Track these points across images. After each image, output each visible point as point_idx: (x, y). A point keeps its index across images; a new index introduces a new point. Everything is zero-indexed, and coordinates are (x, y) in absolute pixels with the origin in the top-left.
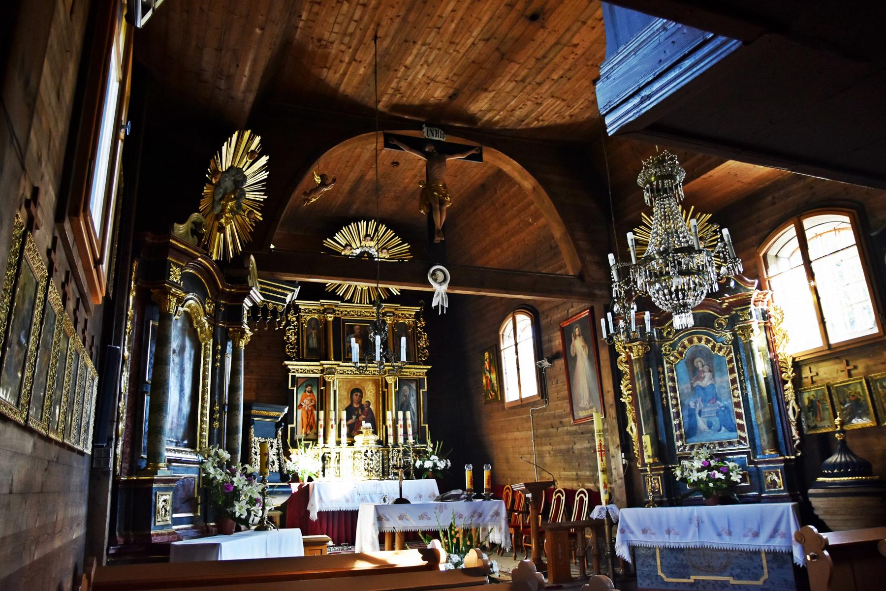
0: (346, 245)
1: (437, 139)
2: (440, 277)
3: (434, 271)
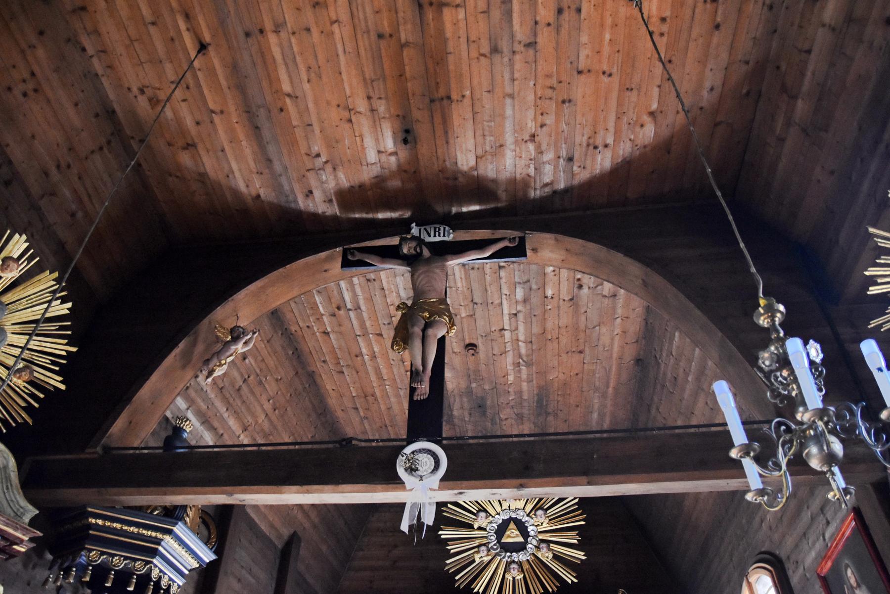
0: (479, 511)
1: (437, 239)
2: (425, 463)
3: (421, 451)
